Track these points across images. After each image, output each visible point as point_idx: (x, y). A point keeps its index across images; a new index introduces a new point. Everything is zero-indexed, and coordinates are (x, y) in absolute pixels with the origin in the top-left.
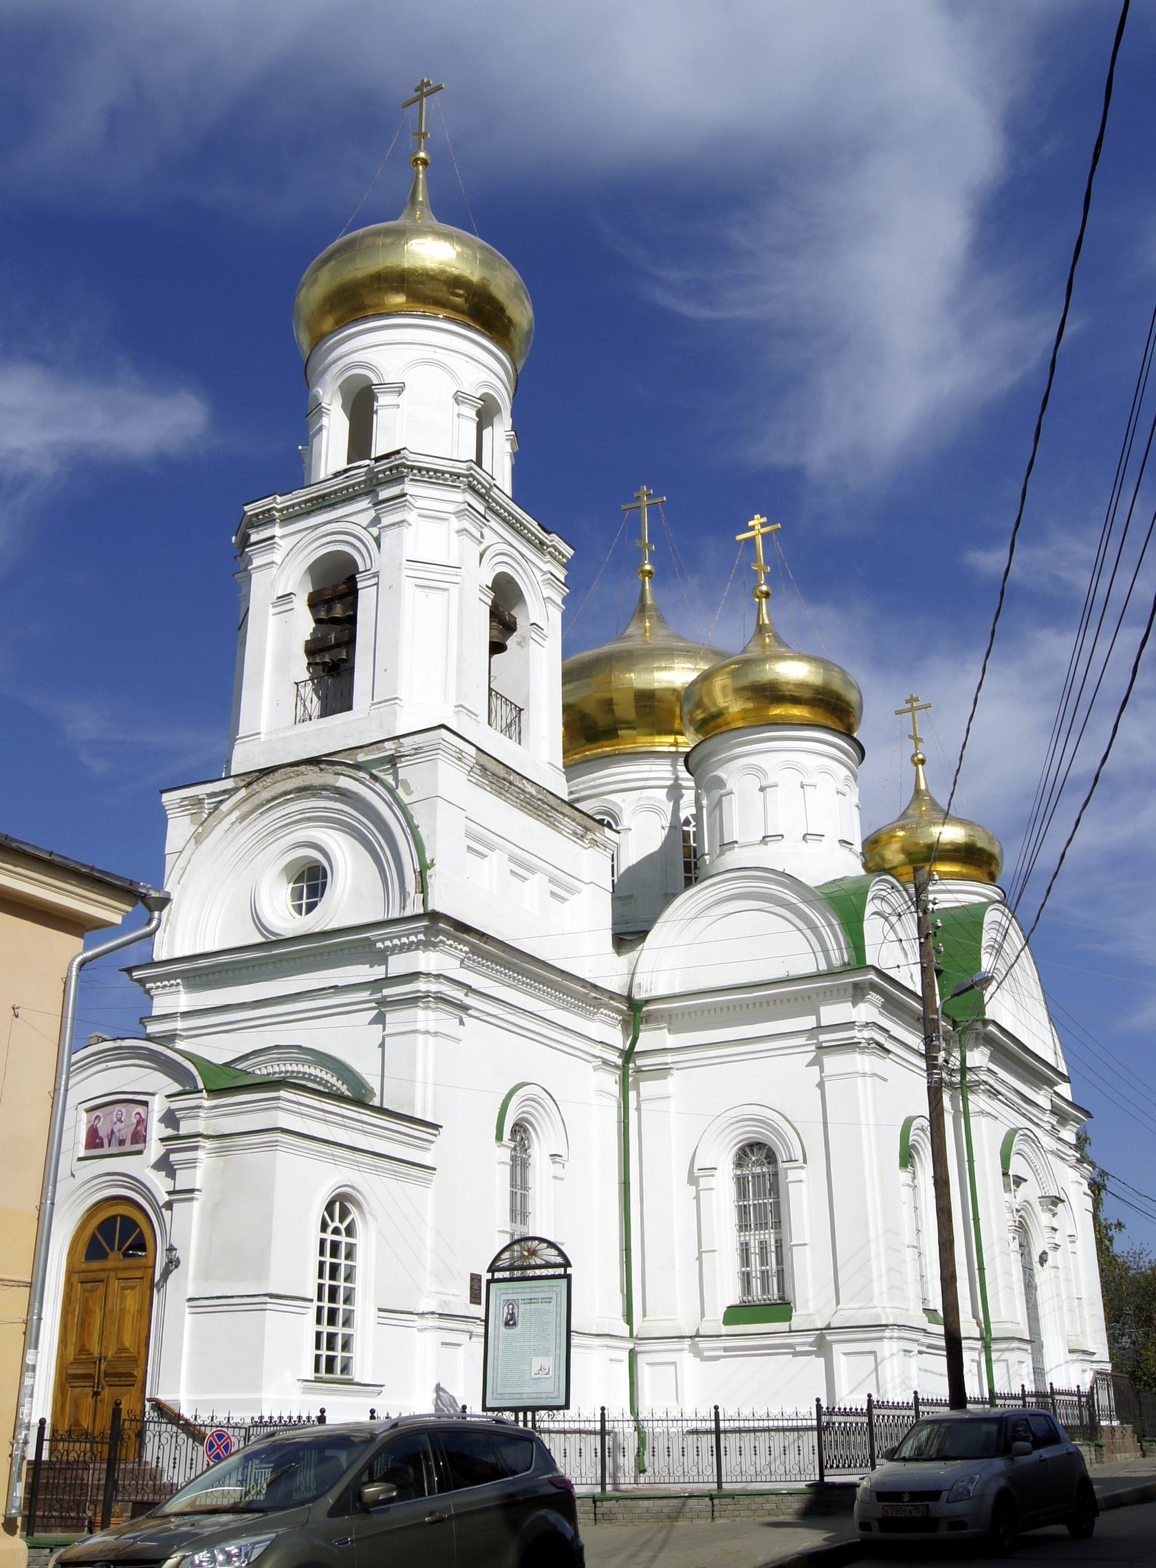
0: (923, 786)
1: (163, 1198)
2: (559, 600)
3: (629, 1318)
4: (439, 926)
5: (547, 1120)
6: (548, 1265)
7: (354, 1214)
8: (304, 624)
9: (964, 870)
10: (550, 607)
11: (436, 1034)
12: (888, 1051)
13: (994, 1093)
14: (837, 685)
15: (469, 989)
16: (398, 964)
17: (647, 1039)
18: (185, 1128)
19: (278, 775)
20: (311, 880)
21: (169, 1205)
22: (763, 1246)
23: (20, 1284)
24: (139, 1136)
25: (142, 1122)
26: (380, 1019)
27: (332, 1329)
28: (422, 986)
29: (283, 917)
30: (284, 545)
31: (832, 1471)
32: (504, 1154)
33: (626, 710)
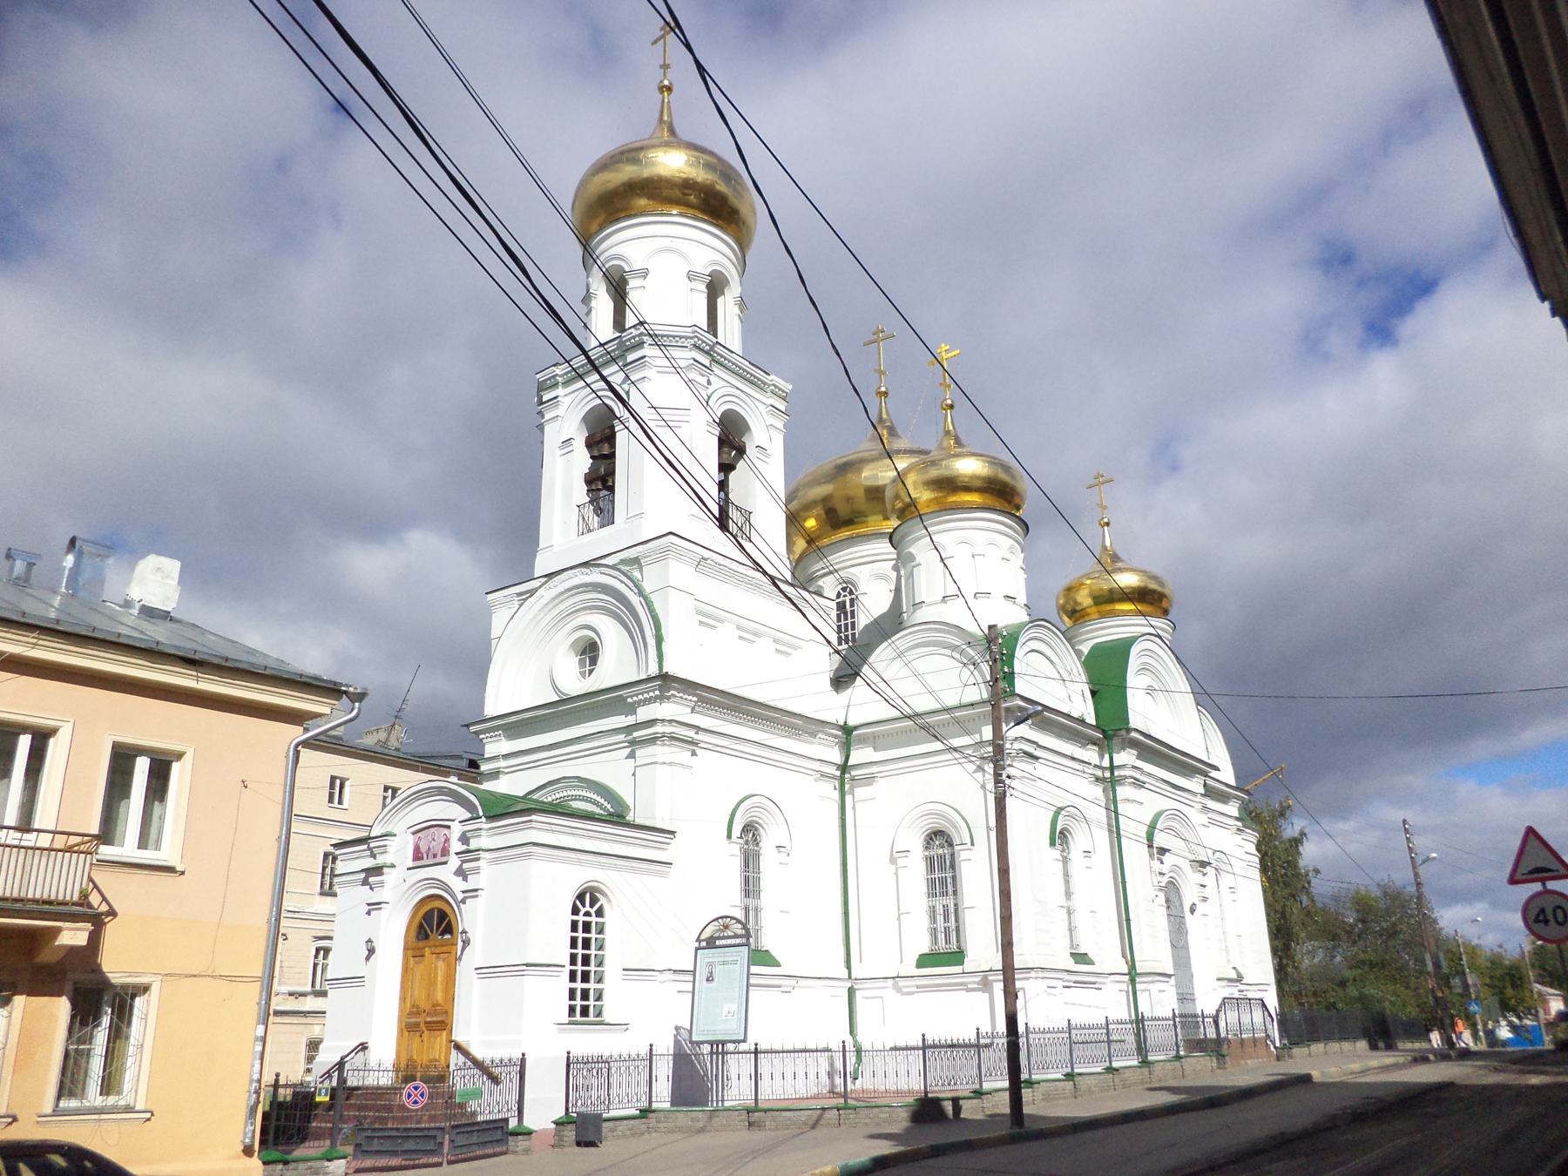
0: (1108, 543)
1: (460, 896)
2: (781, 426)
3: (849, 967)
4: (666, 681)
6: (736, 936)
7: (602, 901)
8: (582, 461)
10: (772, 432)
11: (671, 764)
12: (1037, 758)
13: (1139, 784)
14: (1003, 476)
15: (698, 729)
16: (644, 714)
17: (858, 755)
18: (473, 844)
20: (590, 652)
21: (463, 901)
23: (253, 979)
24: (445, 852)
25: (447, 840)
26: (632, 755)
27: (585, 986)
28: (659, 729)
29: (574, 683)
30: (565, 402)
33: (861, 502)
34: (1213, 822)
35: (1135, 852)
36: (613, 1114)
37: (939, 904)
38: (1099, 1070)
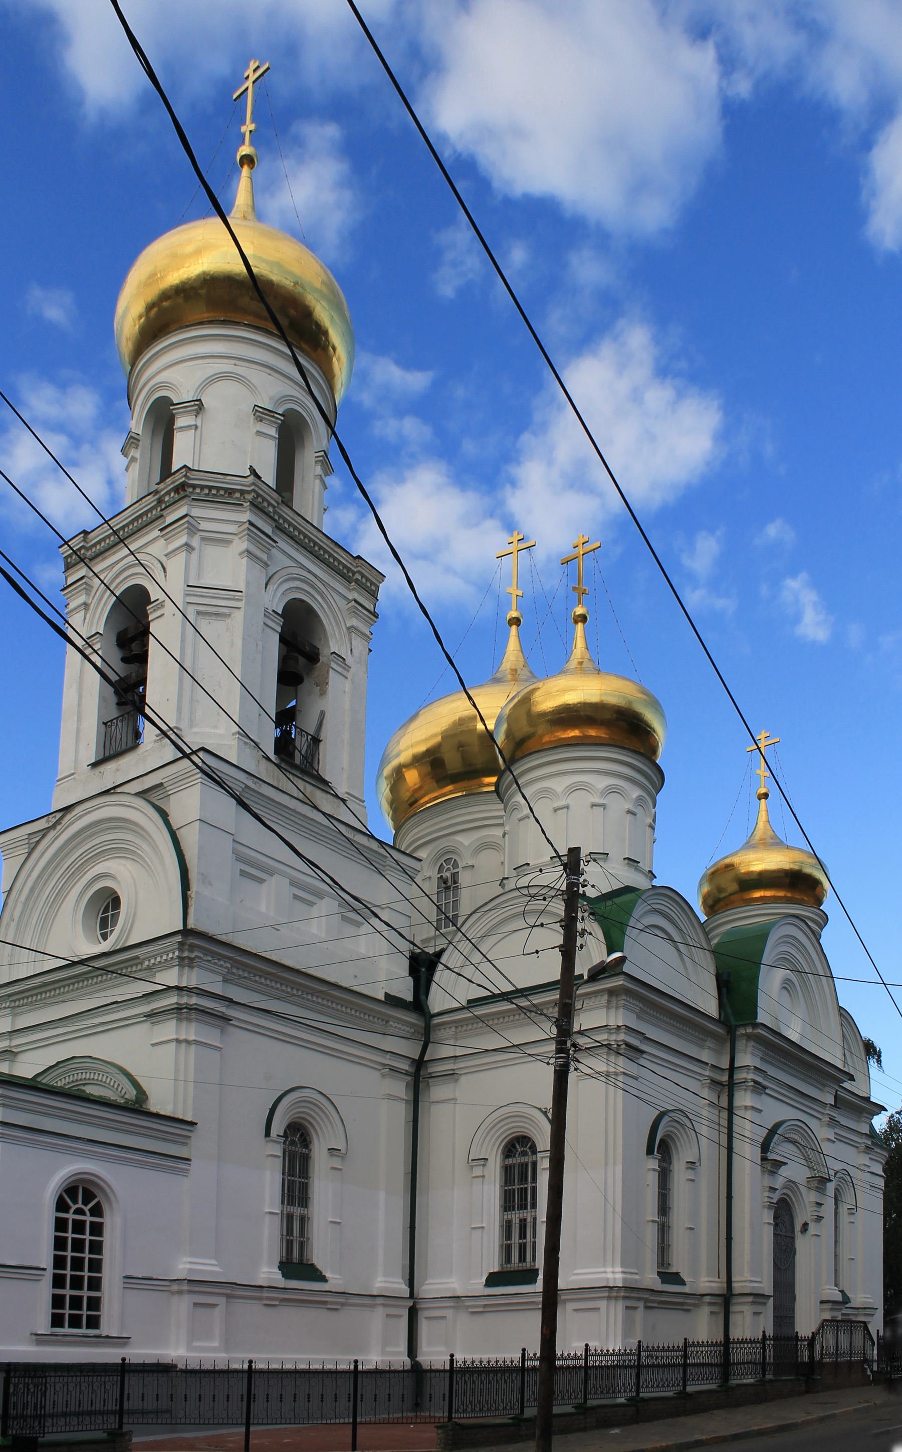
3: (411, 1284)
5: (325, 1119)
9: (789, 895)
12: (643, 1052)
19: (78, 810)
22: (523, 1224)
31: (734, 1377)
32: (653, 1164)
34: (840, 1139)
35: (747, 1153)
36: (49, 1438)
37: (515, 1217)
38: (671, 1394)
